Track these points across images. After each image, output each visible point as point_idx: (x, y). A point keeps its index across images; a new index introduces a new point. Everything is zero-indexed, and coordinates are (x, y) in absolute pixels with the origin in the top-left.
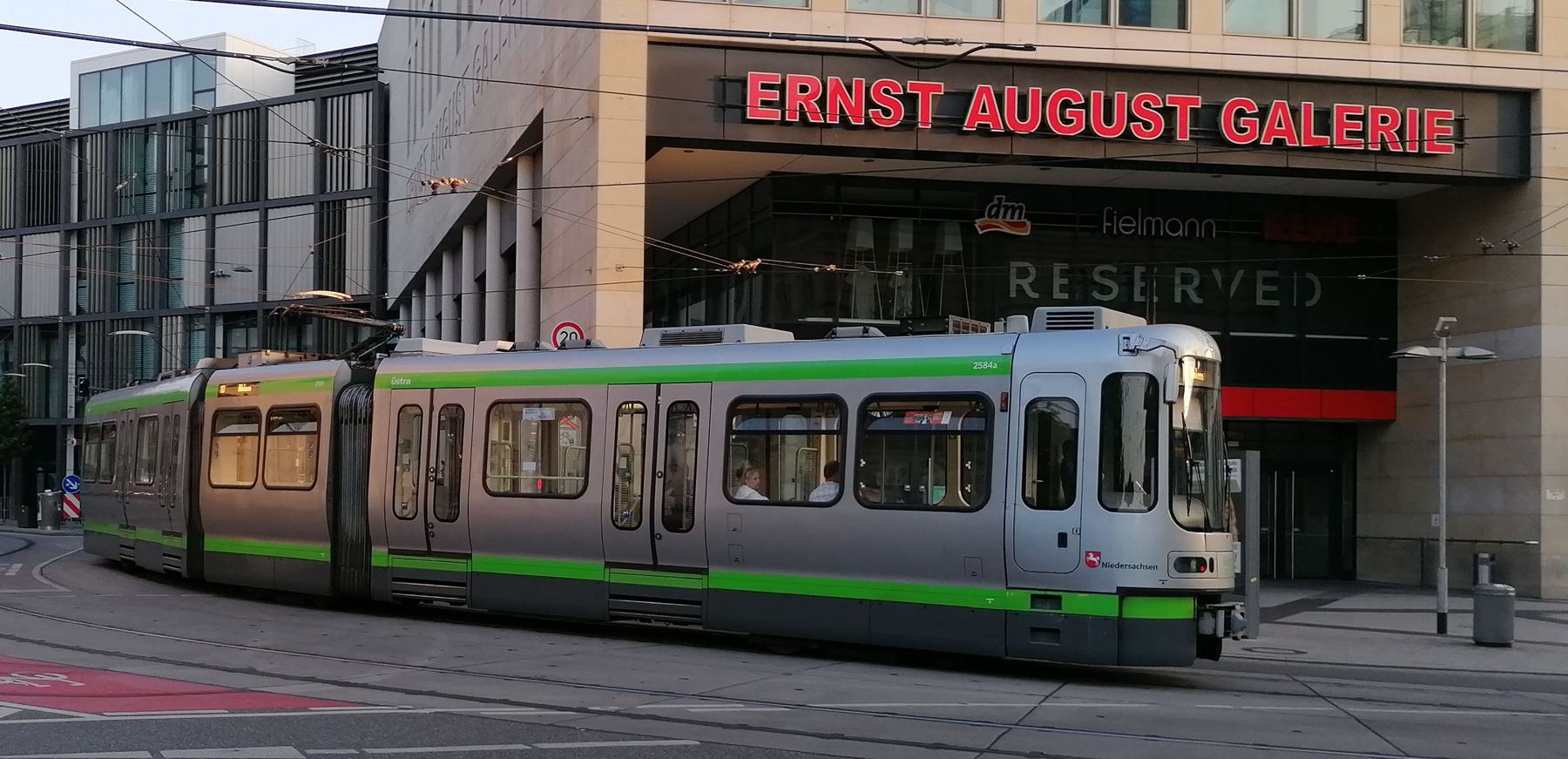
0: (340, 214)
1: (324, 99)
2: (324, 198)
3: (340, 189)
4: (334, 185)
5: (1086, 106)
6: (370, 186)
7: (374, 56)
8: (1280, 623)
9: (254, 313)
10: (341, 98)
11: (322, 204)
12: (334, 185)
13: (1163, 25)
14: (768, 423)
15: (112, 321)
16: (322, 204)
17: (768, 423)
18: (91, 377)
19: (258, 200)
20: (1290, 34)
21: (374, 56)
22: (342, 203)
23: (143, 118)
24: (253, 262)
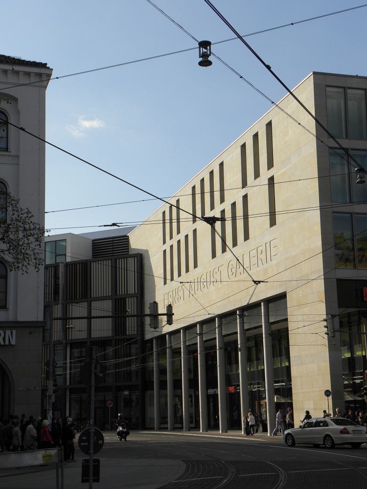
0: (124, 301)
1: (116, 260)
2: (116, 297)
3: (123, 293)
4: (121, 292)
6: (136, 292)
7: (127, 250)
8: (311, 444)
9: (111, 340)
10: (107, 261)
11: (116, 299)
12: (121, 292)
13: (52, 72)
14: (261, 215)
15: (116, 340)
16: (116, 299)
17: (261, 215)
18: (45, 381)
19: (87, 297)
20: (355, 268)
21: (127, 250)
22: (124, 299)
23: (54, 263)
24: (249, 266)
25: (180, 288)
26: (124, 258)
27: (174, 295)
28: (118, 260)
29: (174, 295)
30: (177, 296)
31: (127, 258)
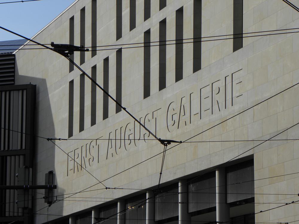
21: (13, 66)
25: (94, 143)
26: (6, 92)
27: (84, 155)
28: (3, 94)
29: (84, 155)
30: (89, 156)
31: (10, 91)
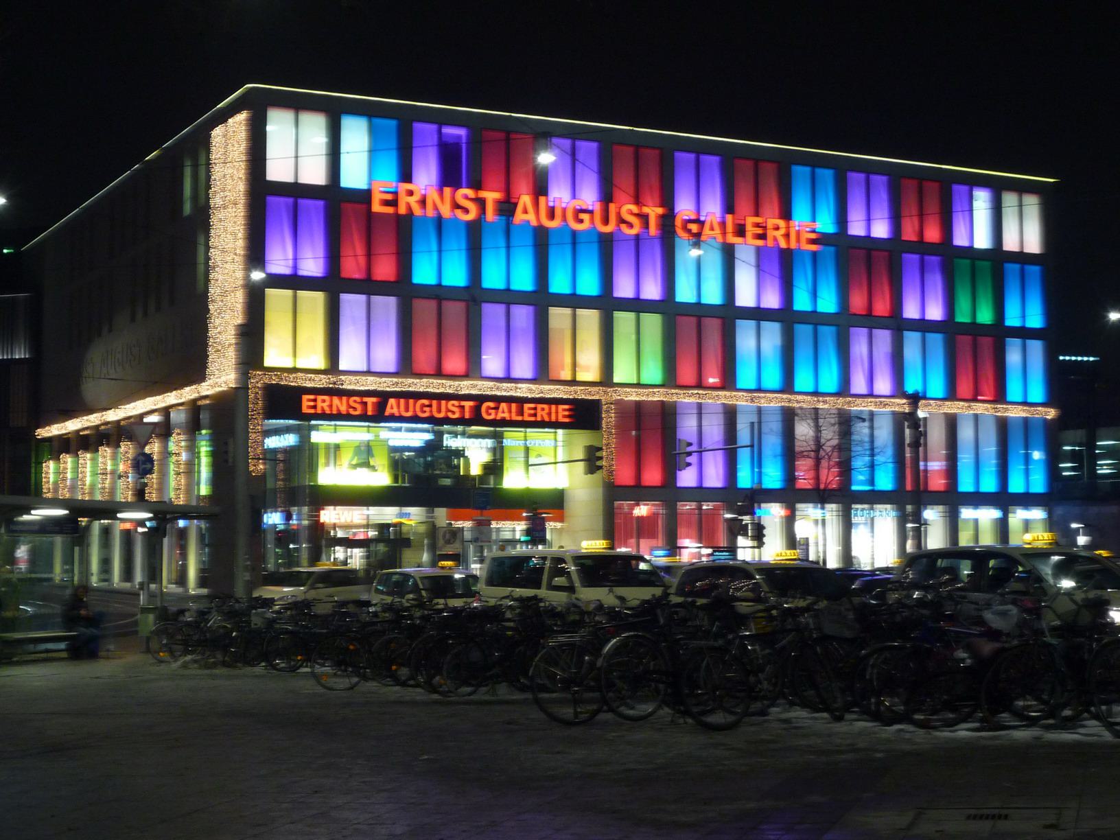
5: (430, 406)
